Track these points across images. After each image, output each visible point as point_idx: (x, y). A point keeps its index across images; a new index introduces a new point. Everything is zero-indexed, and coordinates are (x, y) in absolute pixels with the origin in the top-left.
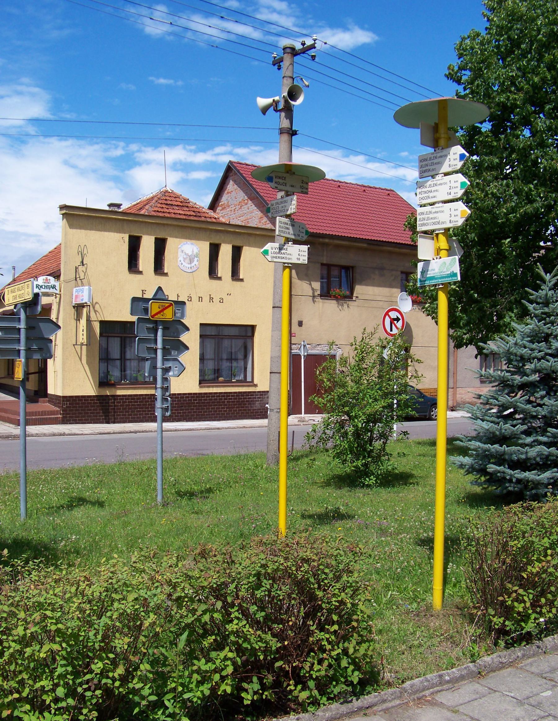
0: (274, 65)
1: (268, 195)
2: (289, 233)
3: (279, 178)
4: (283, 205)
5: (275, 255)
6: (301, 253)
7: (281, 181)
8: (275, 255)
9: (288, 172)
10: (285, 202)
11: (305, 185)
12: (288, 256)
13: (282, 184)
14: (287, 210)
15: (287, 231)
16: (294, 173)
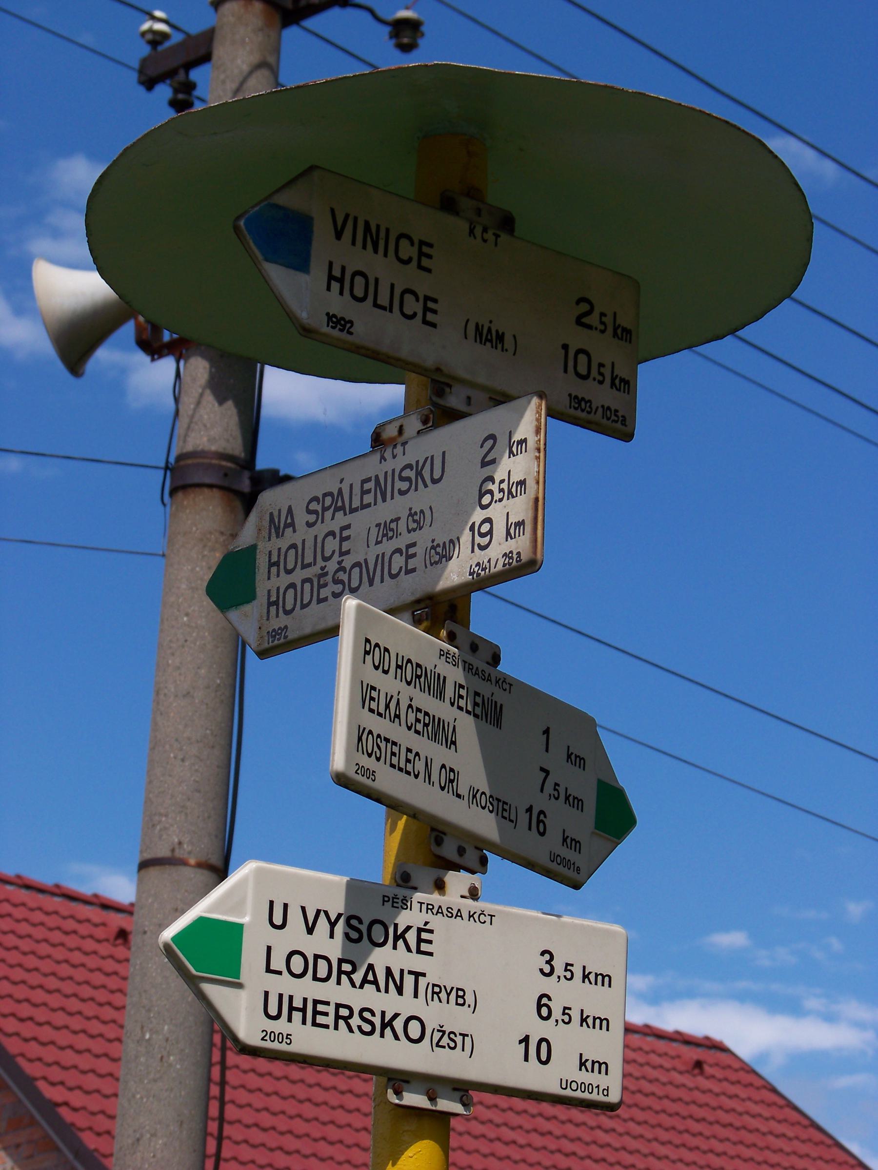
0: (149, 83)
1: (27, 1030)
2: (450, 780)
3: (372, 237)
4: (384, 511)
5: (305, 989)
6: (564, 993)
7: (381, 268)
8: (305, 989)
9: (448, 205)
10: (420, 475)
11: (605, 350)
12: (435, 1014)
13: (396, 303)
14: (443, 553)
15: (438, 753)
16: (507, 223)
